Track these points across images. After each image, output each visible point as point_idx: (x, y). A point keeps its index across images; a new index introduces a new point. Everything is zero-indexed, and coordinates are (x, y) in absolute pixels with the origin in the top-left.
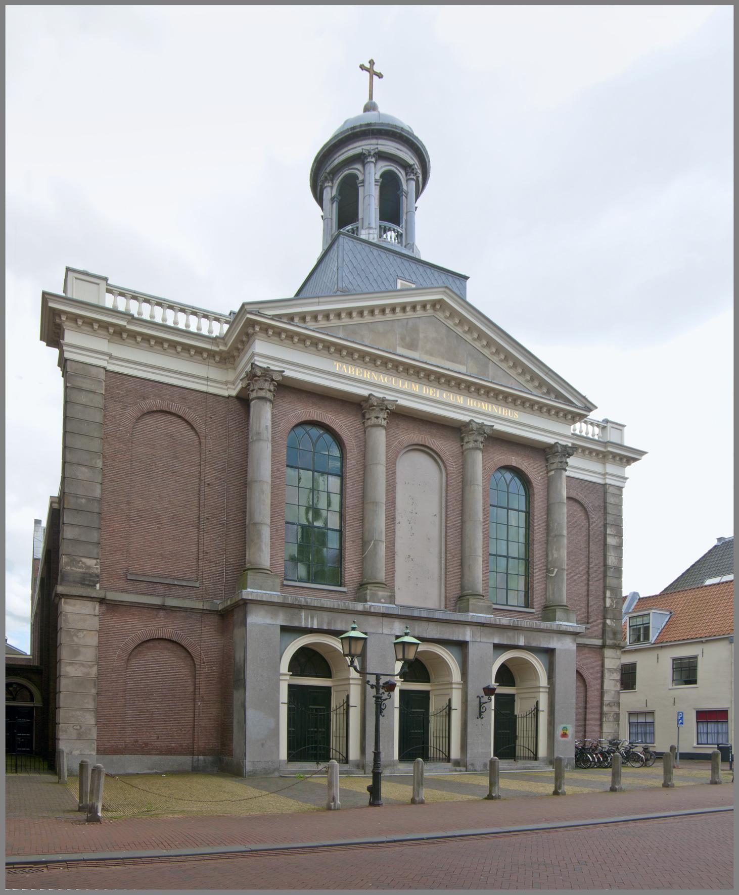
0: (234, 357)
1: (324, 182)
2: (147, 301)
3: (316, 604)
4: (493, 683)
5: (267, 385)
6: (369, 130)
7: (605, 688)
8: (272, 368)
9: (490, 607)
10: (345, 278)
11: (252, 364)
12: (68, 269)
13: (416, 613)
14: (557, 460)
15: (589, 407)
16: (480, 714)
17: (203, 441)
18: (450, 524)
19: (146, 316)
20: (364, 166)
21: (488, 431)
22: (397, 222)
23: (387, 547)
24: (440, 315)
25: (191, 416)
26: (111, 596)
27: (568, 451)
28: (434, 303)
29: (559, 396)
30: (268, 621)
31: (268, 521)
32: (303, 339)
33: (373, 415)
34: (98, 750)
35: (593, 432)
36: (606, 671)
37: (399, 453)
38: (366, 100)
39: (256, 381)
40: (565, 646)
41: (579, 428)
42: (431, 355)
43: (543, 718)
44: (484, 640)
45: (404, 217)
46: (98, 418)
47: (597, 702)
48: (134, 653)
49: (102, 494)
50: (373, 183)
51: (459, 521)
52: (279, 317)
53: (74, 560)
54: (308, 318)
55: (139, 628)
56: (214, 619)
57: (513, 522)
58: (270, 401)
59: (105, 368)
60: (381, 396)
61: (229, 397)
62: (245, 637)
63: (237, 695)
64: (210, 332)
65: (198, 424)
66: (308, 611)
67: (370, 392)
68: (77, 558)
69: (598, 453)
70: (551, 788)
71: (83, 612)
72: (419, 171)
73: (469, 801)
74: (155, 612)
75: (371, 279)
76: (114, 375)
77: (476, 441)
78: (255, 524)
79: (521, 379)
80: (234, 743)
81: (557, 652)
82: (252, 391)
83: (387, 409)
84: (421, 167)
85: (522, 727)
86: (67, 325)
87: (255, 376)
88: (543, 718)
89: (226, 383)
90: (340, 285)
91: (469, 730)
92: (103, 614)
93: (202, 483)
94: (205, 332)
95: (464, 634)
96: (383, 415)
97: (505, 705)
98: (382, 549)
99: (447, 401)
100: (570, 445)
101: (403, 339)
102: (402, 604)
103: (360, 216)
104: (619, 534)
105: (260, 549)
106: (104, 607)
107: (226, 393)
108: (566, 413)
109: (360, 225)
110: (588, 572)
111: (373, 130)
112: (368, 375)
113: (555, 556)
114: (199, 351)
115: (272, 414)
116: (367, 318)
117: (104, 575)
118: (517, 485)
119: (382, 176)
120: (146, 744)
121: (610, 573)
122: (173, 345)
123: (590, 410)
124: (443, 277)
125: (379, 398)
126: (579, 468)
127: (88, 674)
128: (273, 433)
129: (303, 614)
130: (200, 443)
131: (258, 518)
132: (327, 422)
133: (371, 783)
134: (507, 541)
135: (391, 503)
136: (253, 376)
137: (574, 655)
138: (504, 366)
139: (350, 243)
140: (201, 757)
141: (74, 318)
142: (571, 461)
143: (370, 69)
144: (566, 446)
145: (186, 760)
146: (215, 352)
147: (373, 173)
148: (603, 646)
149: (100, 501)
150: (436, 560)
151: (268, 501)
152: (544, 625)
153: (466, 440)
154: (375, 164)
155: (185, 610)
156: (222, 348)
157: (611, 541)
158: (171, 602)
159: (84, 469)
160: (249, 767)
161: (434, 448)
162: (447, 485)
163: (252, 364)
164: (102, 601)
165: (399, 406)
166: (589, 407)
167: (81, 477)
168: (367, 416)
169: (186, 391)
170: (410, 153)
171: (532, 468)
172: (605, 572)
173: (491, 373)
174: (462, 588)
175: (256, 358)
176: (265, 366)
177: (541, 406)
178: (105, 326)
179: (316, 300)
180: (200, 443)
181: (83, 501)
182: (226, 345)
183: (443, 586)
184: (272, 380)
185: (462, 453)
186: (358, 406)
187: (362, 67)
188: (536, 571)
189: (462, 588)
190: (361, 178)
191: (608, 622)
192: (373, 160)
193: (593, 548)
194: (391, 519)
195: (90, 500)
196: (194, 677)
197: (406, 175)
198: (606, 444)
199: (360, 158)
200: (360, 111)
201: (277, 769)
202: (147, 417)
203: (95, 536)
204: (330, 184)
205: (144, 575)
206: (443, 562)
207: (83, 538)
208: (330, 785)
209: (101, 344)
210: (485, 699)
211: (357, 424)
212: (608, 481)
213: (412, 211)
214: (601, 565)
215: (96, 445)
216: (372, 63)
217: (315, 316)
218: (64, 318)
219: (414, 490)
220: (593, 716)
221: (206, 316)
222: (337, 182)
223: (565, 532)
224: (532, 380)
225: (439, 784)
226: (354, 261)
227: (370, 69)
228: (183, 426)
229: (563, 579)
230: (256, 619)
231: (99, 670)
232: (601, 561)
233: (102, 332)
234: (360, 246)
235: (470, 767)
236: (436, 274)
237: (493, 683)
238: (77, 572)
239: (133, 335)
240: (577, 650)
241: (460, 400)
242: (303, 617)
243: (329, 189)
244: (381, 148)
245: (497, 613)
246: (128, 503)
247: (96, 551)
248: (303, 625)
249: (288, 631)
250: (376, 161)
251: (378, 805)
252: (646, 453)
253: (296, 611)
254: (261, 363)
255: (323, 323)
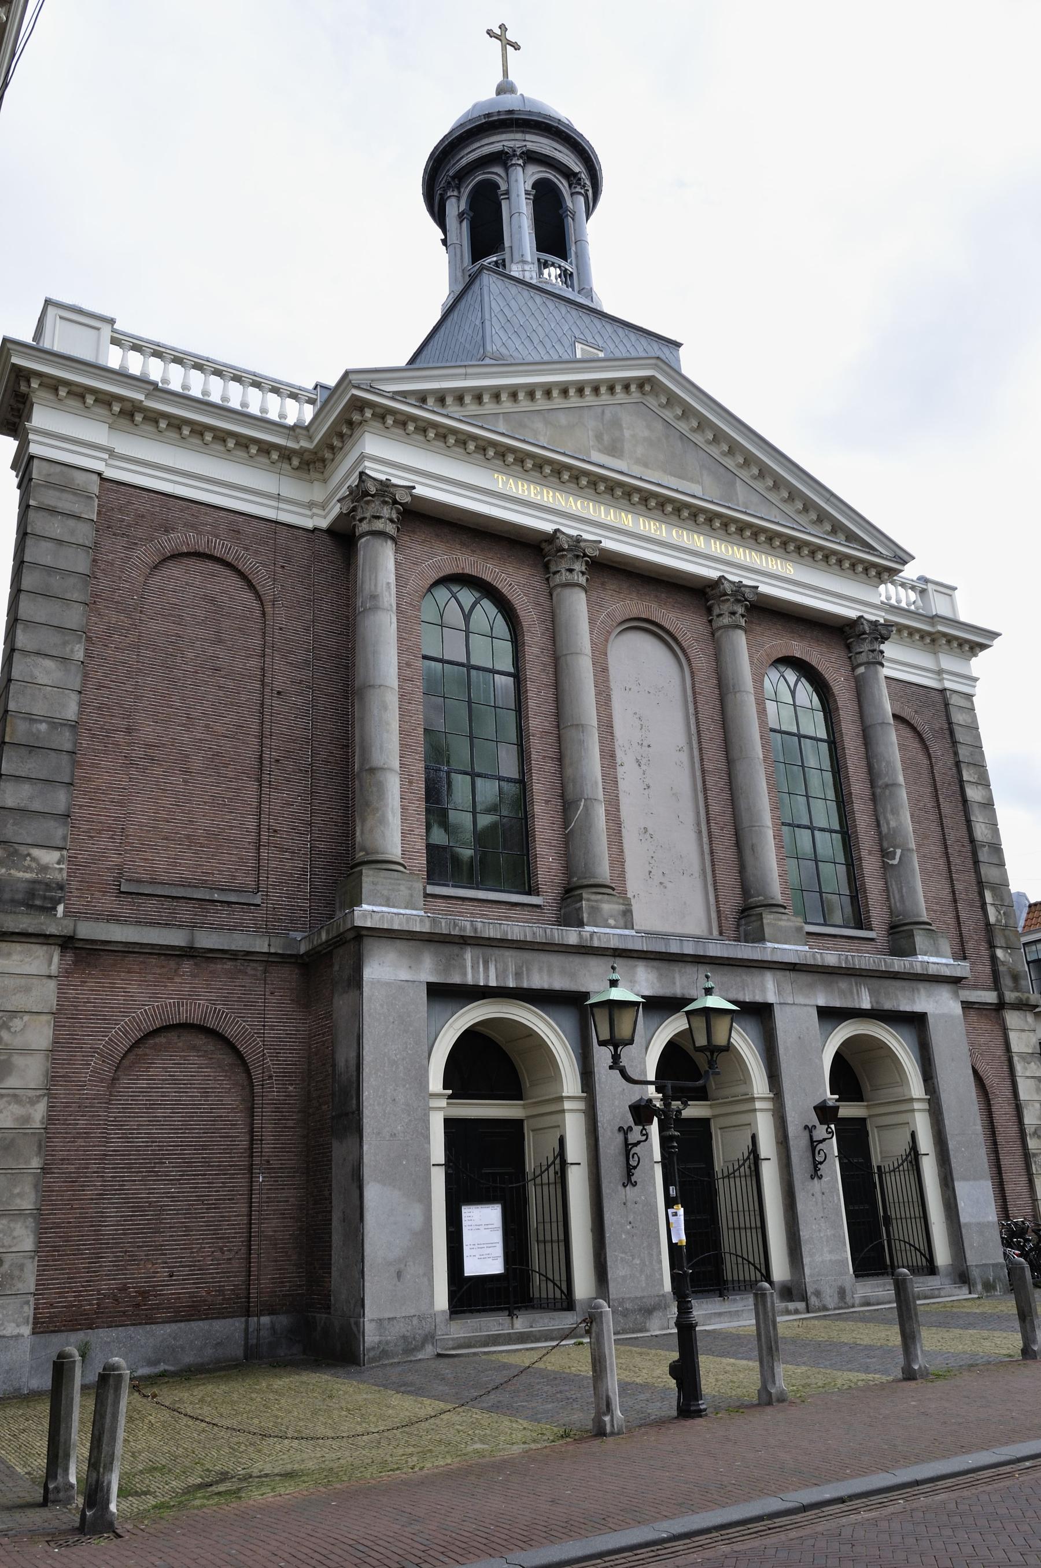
0: (323, 460)
1: (445, 190)
2: (178, 361)
3: (492, 933)
4: (831, 1098)
5: (386, 512)
6: (511, 119)
7: (1023, 1096)
8: (395, 481)
9: (799, 929)
10: (495, 337)
11: (362, 474)
12: (48, 302)
13: (674, 948)
14: (866, 647)
15: (903, 558)
16: (816, 1169)
17: (269, 610)
18: (709, 766)
19: (175, 386)
20: (506, 170)
21: (750, 596)
22: (563, 255)
23: (608, 813)
24: (652, 402)
25: (248, 563)
26: (87, 930)
27: (880, 633)
28: (642, 383)
29: (851, 537)
30: (404, 975)
31: (396, 764)
32: (443, 434)
33: (563, 565)
34: (36, 1322)
35: (906, 598)
36: (1016, 1059)
37: (610, 633)
38: (500, 78)
39: (368, 503)
40: (941, 1006)
41: (887, 592)
42: (646, 465)
43: (929, 1168)
44: (800, 1000)
45: (573, 248)
46: (81, 563)
47: (1013, 1130)
48: (126, 1062)
49: (80, 713)
50: (523, 196)
51: (723, 759)
52: (402, 396)
53: (16, 852)
54: (449, 400)
55: (140, 1000)
56: (288, 975)
57: (812, 762)
58: (392, 538)
59: (100, 474)
60: (574, 533)
61: (315, 529)
62: (357, 1014)
63: (339, 1150)
64: (282, 416)
65: (261, 577)
66: (478, 951)
67: (860, 614)
68: (23, 850)
69: (923, 635)
70: (1015, 1341)
71: (28, 969)
72: (588, 183)
73: (868, 1388)
74: (172, 964)
75: (536, 342)
76: (114, 487)
77: (734, 613)
78: (373, 770)
79: (787, 508)
80: (335, 1273)
81: (931, 1020)
82: (361, 520)
83: (585, 555)
84: (588, 174)
85: (896, 1186)
86: (40, 398)
87: (366, 493)
88: (929, 1168)
89: (311, 505)
90: (489, 348)
91: (800, 1207)
92: (67, 973)
93: (267, 690)
94: (273, 415)
95: (764, 990)
96: (579, 566)
97: (854, 1140)
98: (600, 813)
99: (584, 514)
100: (882, 621)
101: (599, 437)
102: (648, 928)
103: (507, 244)
104: (984, 782)
105: (383, 821)
106: (69, 957)
107: (309, 524)
108: (868, 566)
109: (507, 256)
110: (947, 854)
111: (517, 119)
112: (718, 547)
113: (893, 824)
114: (265, 448)
115: (397, 563)
116: (541, 403)
117: (74, 885)
118: (486, 613)
119: (534, 186)
120: (144, 1294)
121: (984, 855)
122: (199, 430)
123: (905, 563)
124: (643, 341)
125: (733, 583)
126: (901, 662)
127: (28, 1119)
128: (399, 596)
129: (468, 955)
130: (264, 614)
131: (378, 759)
132: (488, 577)
133: (675, 1356)
134: (807, 796)
135: (607, 727)
136: (366, 493)
137: (960, 1027)
138: (758, 485)
139: (499, 283)
140: (265, 1320)
141: (53, 385)
142: (889, 649)
143: (500, 35)
144: (875, 623)
145: (229, 1330)
146: (294, 452)
147: (521, 182)
148: (1001, 1006)
149: (74, 726)
150: (692, 836)
151: (395, 726)
152: (898, 964)
153: (716, 611)
154: (523, 168)
155: (233, 955)
156: (304, 444)
157: (973, 794)
158: (207, 940)
159: (49, 663)
160: (371, 1336)
161: (667, 626)
162: (694, 693)
163: (362, 474)
164: (67, 943)
165: (604, 551)
166: (903, 558)
167: (42, 679)
168: (553, 568)
169: (241, 519)
170: (573, 156)
171: (512, 579)
172: (974, 853)
173: (741, 499)
174: (745, 890)
175: (367, 464)
176: (383, 477)
177: (828, 555)
178: (105, 400)
179: (462, 371)
180: (264, 614)
181: (43, 727)
182: (310, 438)
183: (711, 889)
184: (395, 502)
185: (713, 634)
186: (536, 550)
187: (490, 33)
188: (864, 853)
189: (745, 890)
190: (503, 187)
191: (999, 953)
192: (520, 162)
193: (946, 807)
194: (609, 756)
195: (55, 724)
196: (251, 1112)
197: (570, 186)
198: (934, 619)
199: (502, 158)
200: (492, 94)
201: (430, 1338)
202: (170, 564)
203: (60, 800)
204: (455, 193)
205: (153, 882)
206: (705, 840)
207: (36, 806)
208: (598, 1364)
209: (94, 430)
210: (821, 1132)
211: (537, 582)
212: (948, 685)
213: (580, 241)
214: (966, 841)
215: (74, 617)
216: (503, 27)
217: (459, 397)
218: (35, 384)
219: (635, 698)
220: (1011, 1162)
221: (275, 390)
222: (466, 192)
223: (901, 779)
224: (806, 509)
225: (822, 1352)
226: (506, 310)
227: (500, 35)
228: (233, 582)
229: (914, 870)
230: (385, 973)
231: (50, 1108)
232: (964, 832)
233: (101, 411)
234: (514, 289)
235: (813, 1300)
236: (633, 337)
237: (831, 1098)
238: (19, 879)
239: (153, 418)
240: (964, 1013)
241: (699, 542)
242: (469, 964)
243: (453, 200)
244: (530, 146)
245: (812, 941)
246: (129, 731)
247: (60, 832)
248: (470, 980)
249: (445, 995)
250: (525, 163)
251: (699, 1413)
252: (999, 635)
253: (456, 949)
254: (377, 472)
255: (472, 408)
